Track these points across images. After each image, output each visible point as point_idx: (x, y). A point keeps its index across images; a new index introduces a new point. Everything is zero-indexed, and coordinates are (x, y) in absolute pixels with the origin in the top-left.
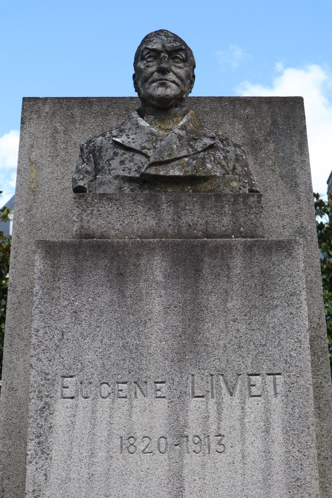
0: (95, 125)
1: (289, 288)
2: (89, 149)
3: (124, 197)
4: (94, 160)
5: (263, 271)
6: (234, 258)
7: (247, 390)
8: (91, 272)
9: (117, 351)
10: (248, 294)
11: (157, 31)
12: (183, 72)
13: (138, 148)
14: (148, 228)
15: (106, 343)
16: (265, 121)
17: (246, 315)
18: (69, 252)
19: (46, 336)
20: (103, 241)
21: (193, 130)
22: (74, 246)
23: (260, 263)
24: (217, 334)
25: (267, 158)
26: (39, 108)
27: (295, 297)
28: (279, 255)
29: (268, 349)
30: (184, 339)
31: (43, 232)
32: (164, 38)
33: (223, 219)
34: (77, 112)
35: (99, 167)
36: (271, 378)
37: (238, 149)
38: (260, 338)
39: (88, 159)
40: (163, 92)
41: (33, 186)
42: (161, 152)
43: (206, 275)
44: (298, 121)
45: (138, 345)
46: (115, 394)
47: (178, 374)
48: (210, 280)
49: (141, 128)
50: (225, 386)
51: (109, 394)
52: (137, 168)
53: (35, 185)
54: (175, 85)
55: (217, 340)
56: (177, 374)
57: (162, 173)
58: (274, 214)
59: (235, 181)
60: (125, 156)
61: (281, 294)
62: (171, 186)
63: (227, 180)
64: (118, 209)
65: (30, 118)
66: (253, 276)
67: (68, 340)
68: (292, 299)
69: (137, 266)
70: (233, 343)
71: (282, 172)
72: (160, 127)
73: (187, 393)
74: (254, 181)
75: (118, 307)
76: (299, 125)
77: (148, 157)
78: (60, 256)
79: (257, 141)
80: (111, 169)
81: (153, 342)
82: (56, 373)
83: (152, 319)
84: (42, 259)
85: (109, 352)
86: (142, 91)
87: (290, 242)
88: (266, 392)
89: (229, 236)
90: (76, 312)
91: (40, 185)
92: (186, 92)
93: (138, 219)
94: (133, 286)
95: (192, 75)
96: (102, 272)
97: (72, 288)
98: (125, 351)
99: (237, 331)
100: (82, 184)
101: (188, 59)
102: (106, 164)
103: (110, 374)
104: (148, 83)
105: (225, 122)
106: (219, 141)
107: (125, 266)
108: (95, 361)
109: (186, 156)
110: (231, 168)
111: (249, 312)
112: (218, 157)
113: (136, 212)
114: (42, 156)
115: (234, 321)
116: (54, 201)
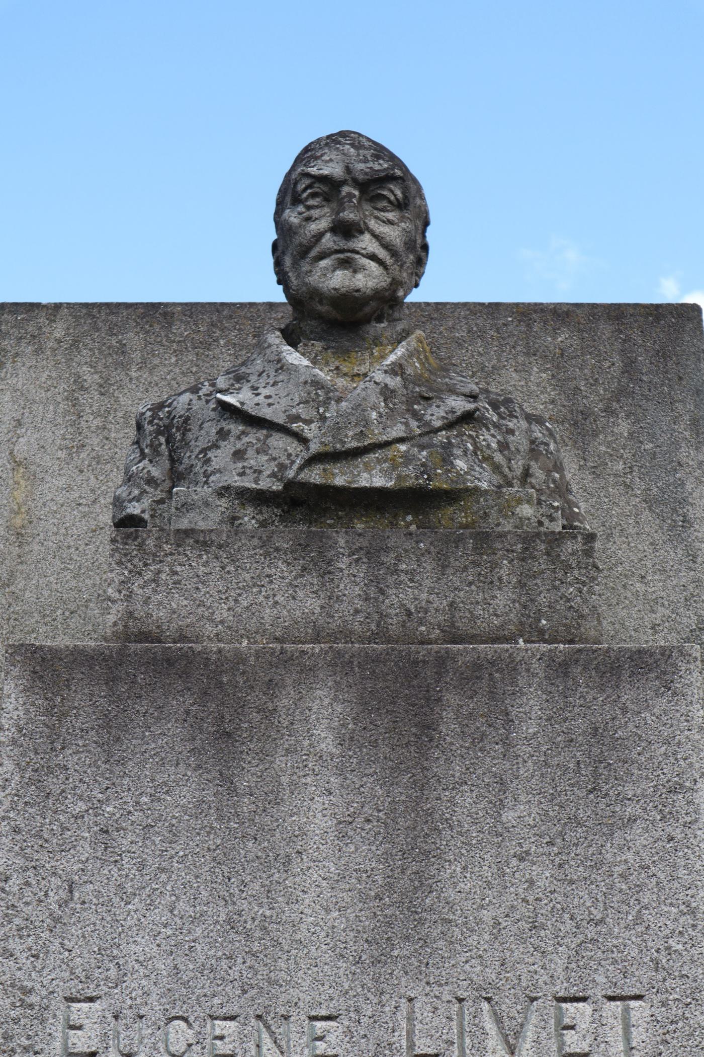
0: (177, 370)
1: (664, 774)
2: (157, 424)
3: (240, 540)
4: (170, 451)
5: (596, 729)
6: (523, 694)
7: (553, 1040)
8: (148, 728)
9: (211, 934)
10: (559, 789)
11: (332, 135)
12: (397, 232)
13: (281, 419)
14: (299, 619)
15: (183, 913)
16: (606, 364)
17: (551, 843)
18: (92, 675)
19: (27, 892)
20: (182, 648)
21: (421, 375)
22: (107, 661)
23: (589, 707)
24: (475, 893)
25: (611, 455)
26: (40, 328)
27: (680, 796)
28: (638, 688)
29: (610, 933)
30: (390, 906)
31: (40, 638)
32: (349, 149)
33: (494, 597)
34: (133, 339)
35: (181, 468)
36: (618, 1007)
37: (535, 427)
38: (589, 904)
39: (155, 448)
40: (347, 283)
41: (18, 521)
42: (337, 428)
43: (448, 738)
44: (689, 363)
45: (268, 920)
46: (203, 1048)
47: (371, 997)
48: (459, 752)
49: (288, 369)
50: (496, 1029)
51: (190, 1045)
52: (276, 470)
53: (23, 520)
54: (377, 265)
55: (474, 907)
56: (369, 995)
57: (339, 481)
58: (629, 595)
59: (528, 502)
60: (246, 440)
61: (643, 789)
62: (362, 515)
63: (507, 500)
64: (223, 568)
65: (17, 354)
66: (572, 741)
67: (84, 903)
68: (674, 801)
69: (268, 713)
70: (518, 917)
71: (650, 490)
72: (337, 368)
73: (394, 1046)
74: (578, 508)
75: (216, 819)
76: (691, 375)
77: (304, 441)
78: (68, 686)
79: (586, 414)
80: (209, 472)
81: (308, 911)
82: (51, 990)
83: (305, 850)
84: (21, 692)
85: (191, 938)
86: (294, 281)
87: (667, 653)
88: (603, 1045)
89: (511, 639)
90: (107, 832)
91: (35, 521)
92: (405, 283)
93: (274, 595)
94: (257, 766)
95: (419, 241)
96: (174, 728)
97: (98, 767)
98: (232, 936)
99: (527, 884)
100: (137, 511)
101: (409, 201)
102: (199, 460)
103: (193, 993)
104: (307, 260)
105: (504, 366)
106: (487, 406)
107: (238, 713)
108: (154, 960)
109: (401, 440)
110: (519, 472)
111: (561, 834)
112: (484, 443)
113: (269, 576)
114: (43, 447)
115: (522, 859)
116: (71, 559)
